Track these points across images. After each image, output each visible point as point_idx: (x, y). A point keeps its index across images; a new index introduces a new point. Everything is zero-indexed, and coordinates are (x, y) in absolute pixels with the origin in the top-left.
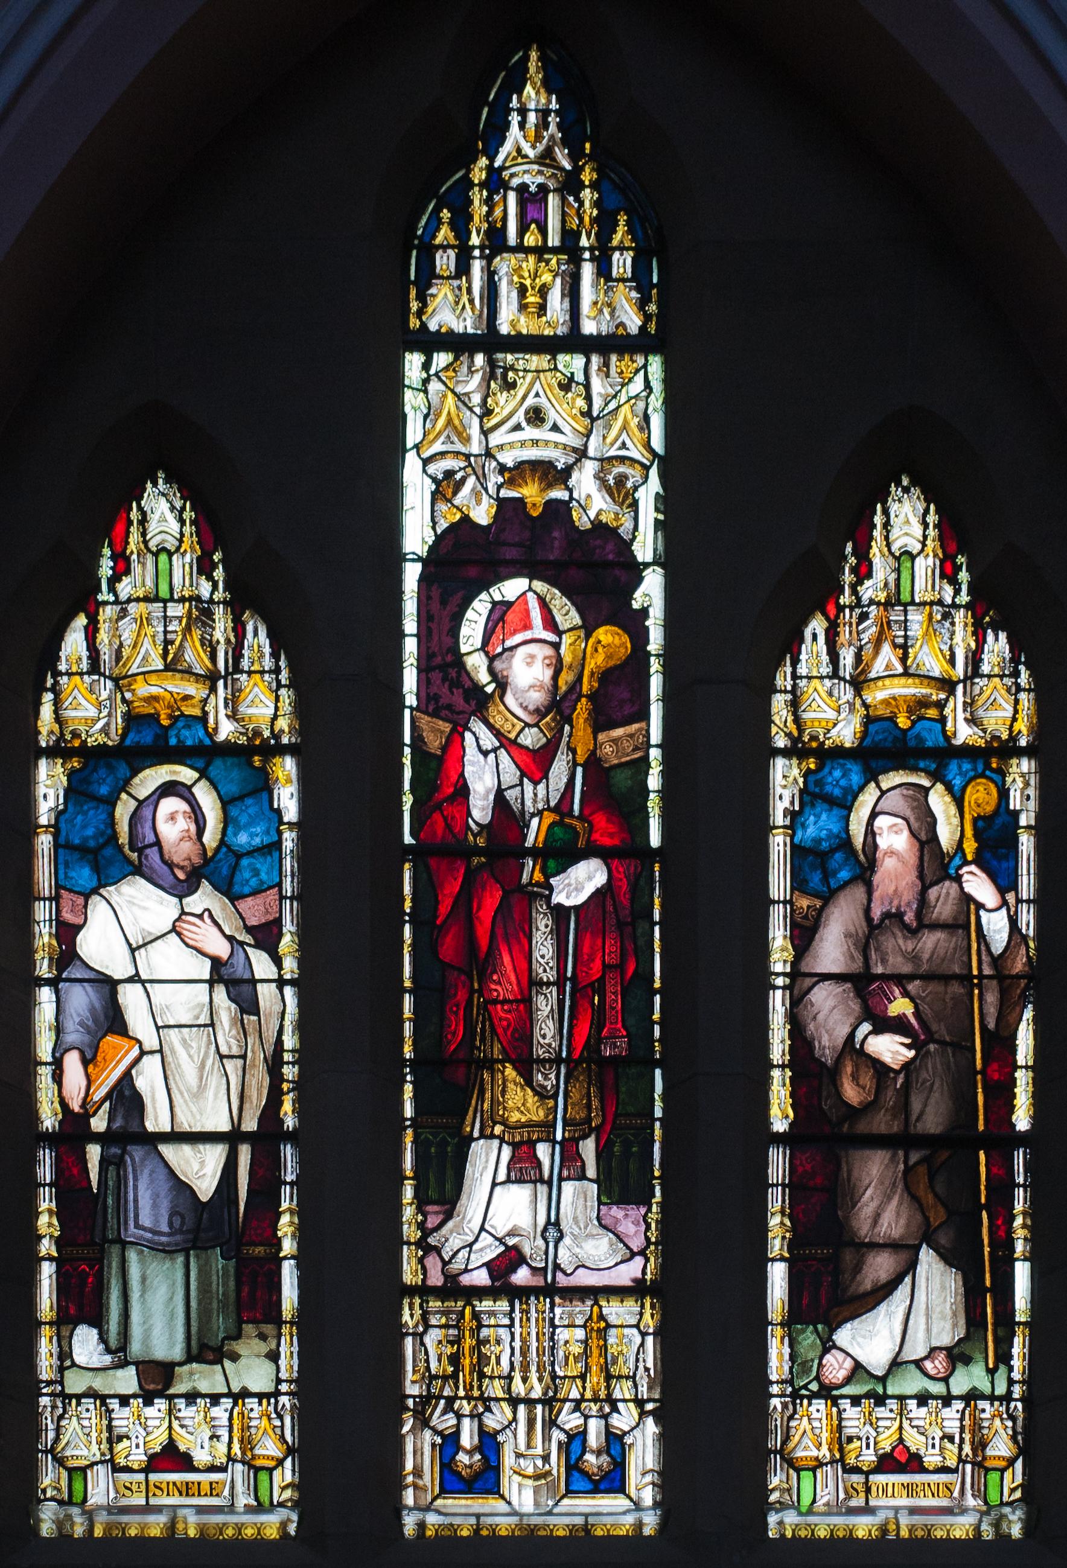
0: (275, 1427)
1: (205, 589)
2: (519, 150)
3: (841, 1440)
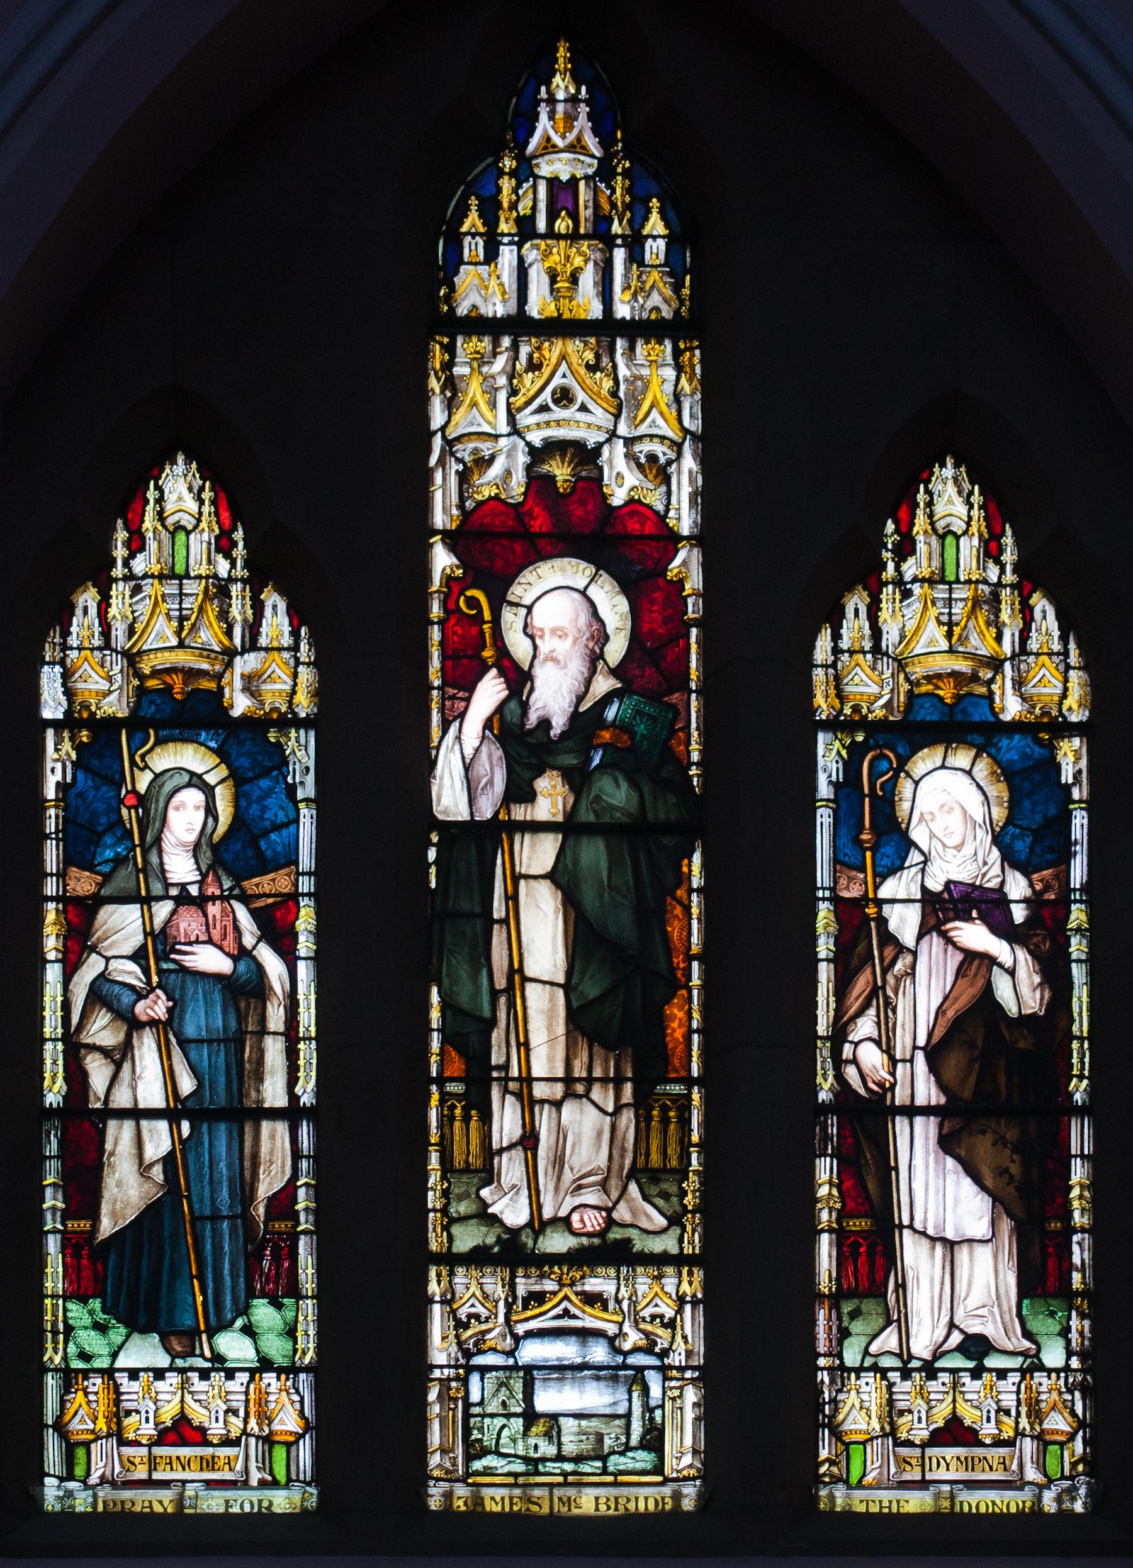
0: (1065, 1401)
1: (223, 567)
2: (549, 139)
3: (891, 1410)
